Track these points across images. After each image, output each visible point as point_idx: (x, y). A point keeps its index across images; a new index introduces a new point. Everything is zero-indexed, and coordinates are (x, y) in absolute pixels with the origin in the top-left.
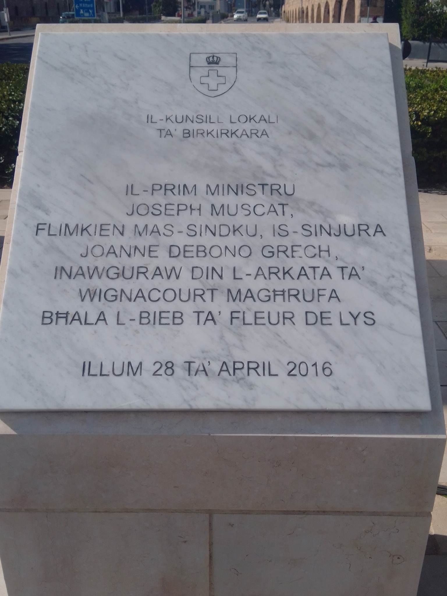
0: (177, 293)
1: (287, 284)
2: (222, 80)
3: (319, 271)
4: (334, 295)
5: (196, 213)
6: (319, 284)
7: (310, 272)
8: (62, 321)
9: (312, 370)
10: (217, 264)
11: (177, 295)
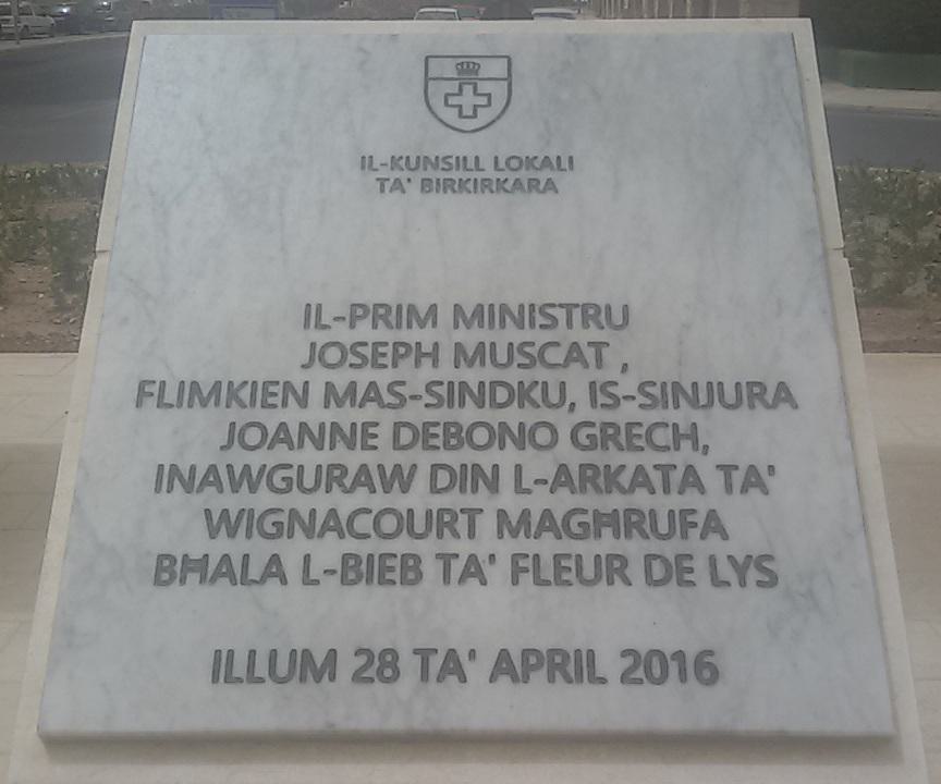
0: (255, 531)
1: (615, 502)
2: (484, 101)
3: (676, 477)
4: (714, 524)
5: (427, 362)
6: (675, 502)
7: (656, 478)
8: (193, 578)
9: (673, 668)
10: (486, 460)
11: (406, 522)
